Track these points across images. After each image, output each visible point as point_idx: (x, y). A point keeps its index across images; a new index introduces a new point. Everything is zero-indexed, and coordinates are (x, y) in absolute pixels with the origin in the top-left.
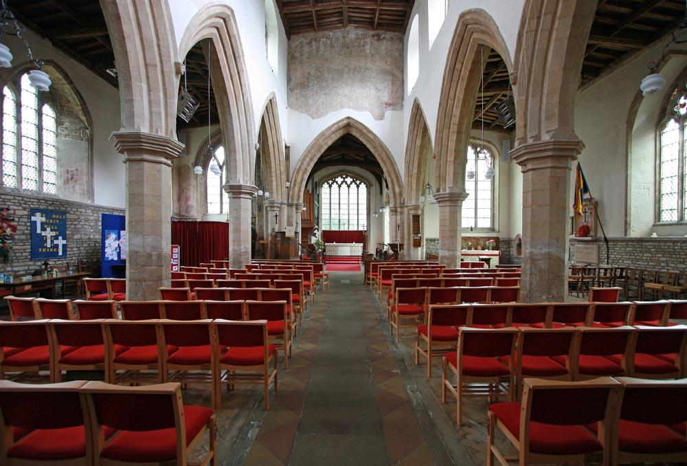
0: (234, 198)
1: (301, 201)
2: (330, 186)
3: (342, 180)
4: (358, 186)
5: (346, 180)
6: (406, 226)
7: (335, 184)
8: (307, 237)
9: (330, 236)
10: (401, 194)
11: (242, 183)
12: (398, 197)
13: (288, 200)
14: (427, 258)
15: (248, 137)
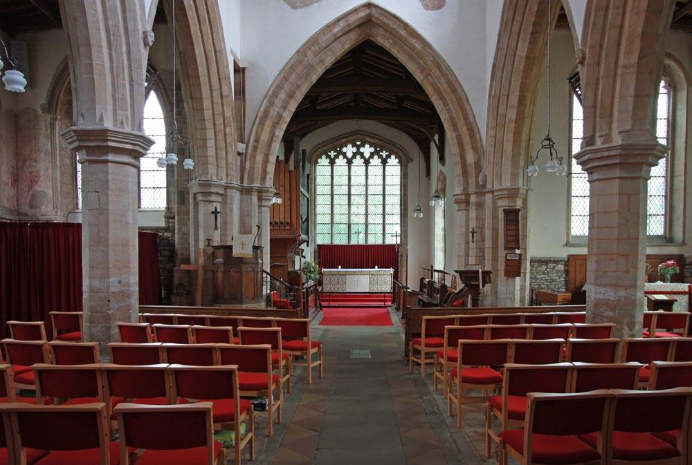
0: (90, 162)
1: (269, 183)
2: (332, 162)
3: (355, 150)
4: (384, 162)
5: (362, 150)
6: (488, 233)
7: (341, 157)
8: (285, 257)
9: (330, 256)
10: (478, 166)
11: (108, 124)
12: (472, 172)
13: (242, 182)
14: (531, 303)
15: (124, 11)
